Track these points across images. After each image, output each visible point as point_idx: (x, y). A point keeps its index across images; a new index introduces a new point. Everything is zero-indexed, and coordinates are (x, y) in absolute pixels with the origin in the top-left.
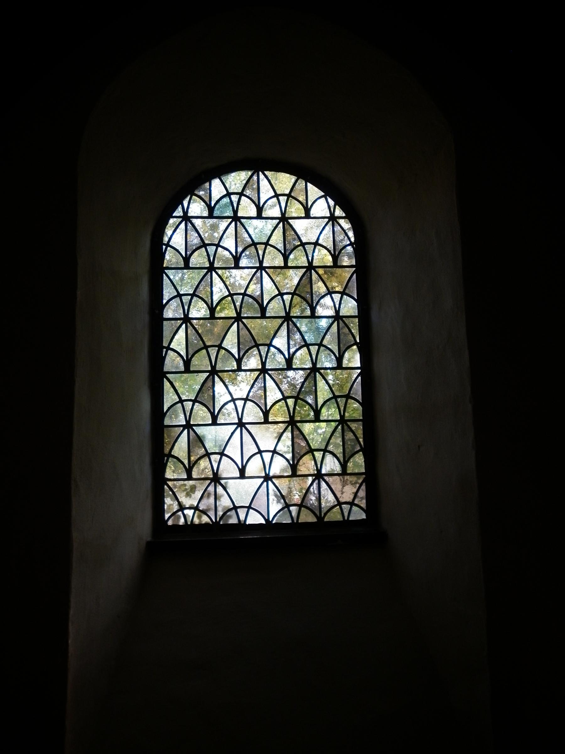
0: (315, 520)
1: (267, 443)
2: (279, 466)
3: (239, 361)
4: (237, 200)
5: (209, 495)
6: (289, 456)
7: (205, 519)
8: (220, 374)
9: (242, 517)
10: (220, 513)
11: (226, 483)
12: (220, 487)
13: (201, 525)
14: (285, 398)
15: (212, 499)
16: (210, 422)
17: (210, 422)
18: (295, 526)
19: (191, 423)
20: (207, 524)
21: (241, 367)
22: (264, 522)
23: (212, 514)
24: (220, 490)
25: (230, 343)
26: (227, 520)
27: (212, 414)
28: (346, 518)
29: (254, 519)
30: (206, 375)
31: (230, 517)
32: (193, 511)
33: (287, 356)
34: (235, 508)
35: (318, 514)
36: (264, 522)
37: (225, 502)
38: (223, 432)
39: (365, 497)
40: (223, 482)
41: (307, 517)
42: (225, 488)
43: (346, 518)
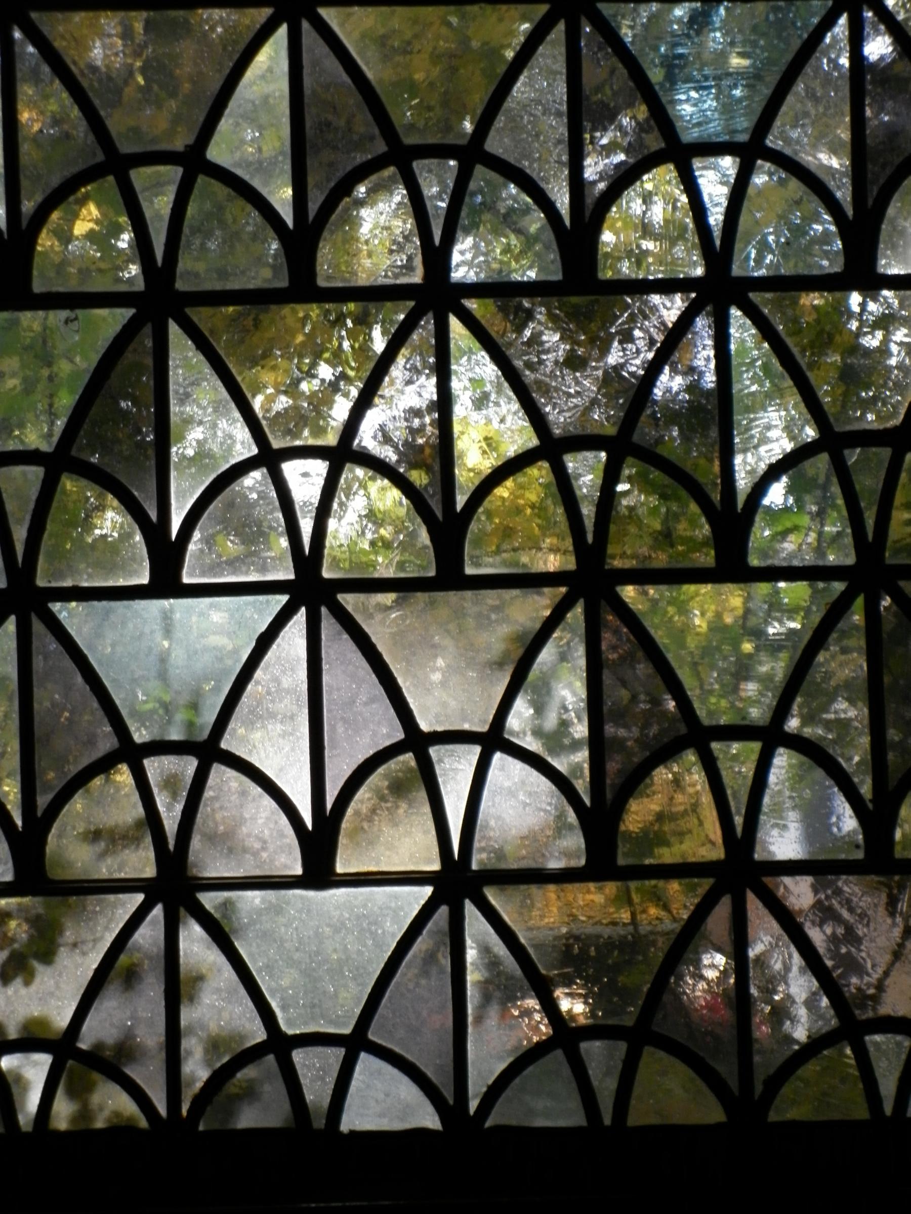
0: (712, 1113)
1: (444, 693)
2: (519, 808)
3: (302, 241)
4: (748, 769)
5: (131, 978)
6: (575, 761)
7: (112, 1102)
8: (200, 315)
9: (317, 1091)
10: (197, 1070)
11: (227, 905)
12: (197, 929)
13: (82, 1137)
14: (551, 448)
15: (153, 991)
16: (144, 579)
17: (144, 579)
18: (606, 1146)
19: (41, 583)
20: (121, 1130)
21: (312, 273)
22: (430, 1120)
23: (150, 1077)
24: (194, 941)
25: (253, 136)
26: (230, 1113)
27: (155, 532)
28: (888, 1109)
29: (383, 1102)
30: (112, 320)
31: (250, 1093)
32: (44, 1060)
33: (562, 201)
34: (279, 1044)
35: (733, 1083)
36: (430, 1120)
37: (219, 1010)
38: (208, 631)
39: (121, 14)
40: (209, 900)
41: (672, 1096)
42: (221, 936)
43: (888, 1109)
